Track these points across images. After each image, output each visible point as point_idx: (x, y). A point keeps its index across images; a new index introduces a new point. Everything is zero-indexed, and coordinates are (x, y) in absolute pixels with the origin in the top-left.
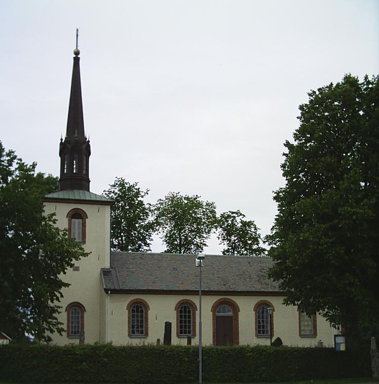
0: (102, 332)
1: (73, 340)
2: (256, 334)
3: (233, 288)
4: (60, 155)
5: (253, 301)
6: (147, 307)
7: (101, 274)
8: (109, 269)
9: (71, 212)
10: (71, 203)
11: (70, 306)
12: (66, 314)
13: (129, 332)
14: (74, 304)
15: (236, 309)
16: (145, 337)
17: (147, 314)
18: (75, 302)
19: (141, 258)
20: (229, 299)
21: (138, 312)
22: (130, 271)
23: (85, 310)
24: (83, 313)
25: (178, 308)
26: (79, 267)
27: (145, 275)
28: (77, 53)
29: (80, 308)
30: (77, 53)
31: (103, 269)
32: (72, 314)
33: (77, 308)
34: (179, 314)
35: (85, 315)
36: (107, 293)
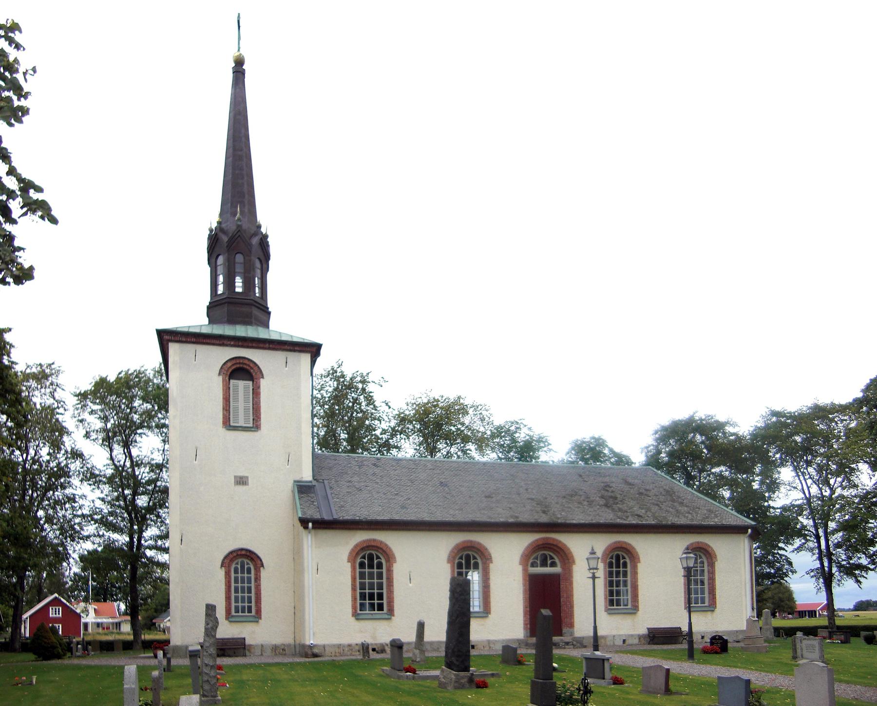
0: (297, 613)
1: (239, 625)
2: (606, 607)
3: (561, 517)
4: (208, 316)
5: (601, 543)
6: (390, 557)
7: (293, 491)
8: (311, 482)
9: (229, 364)
10: (227, 345)
11: (231, 556)
12: (223, 573)
13: (354, 607)
14: (239, 553)
15: (566, 558)
16: (387, 617)
17: (390, 571)
18: (242, 549)
19: (374, 465)
20: (554, 539)
21: (371, 566)
22: (354, 486)
23: (262, 565)
24: (258, 571)
25: (454, 558)
26: (247, 477)
27: (385, 494)
28: (239, 63)
29: (252, 559)
30: (239, 63)
31: (298, 482)
32: (236, 572)
33: (246, 561)
34: (456, 570)
35: (263, 574)
36: (306, 528)
